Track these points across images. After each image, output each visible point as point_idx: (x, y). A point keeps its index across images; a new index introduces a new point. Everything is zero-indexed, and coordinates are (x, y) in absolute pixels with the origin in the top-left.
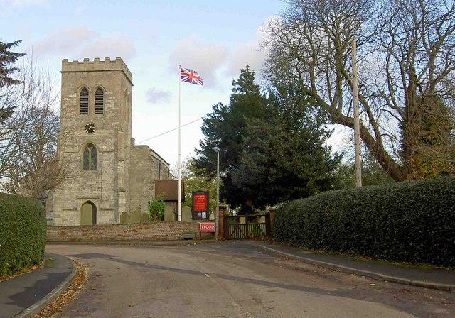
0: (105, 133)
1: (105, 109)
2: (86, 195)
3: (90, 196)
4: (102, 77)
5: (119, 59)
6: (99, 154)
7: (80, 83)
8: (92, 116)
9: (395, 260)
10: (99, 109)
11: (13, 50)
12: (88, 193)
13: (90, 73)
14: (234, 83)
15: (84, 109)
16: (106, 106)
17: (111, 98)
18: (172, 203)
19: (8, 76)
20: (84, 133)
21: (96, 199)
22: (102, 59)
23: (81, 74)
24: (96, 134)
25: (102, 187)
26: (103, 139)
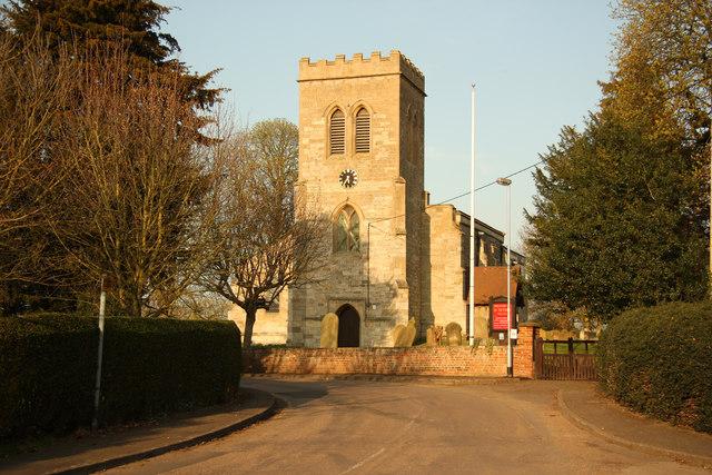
0: (374, 186)
1: (373, 146)
2: (341, 295)
3: (348, 296)
4: (338, 90)
7: (331, 100)
8: (348, 161)
9: (380, 180)
10: (362, 146)
11: (209, 86)
13: (347, 81)
14: (220, 101)
16: (374, 139)
17: (382, 124)
18: (483, 308)
19: (203, 131)
20: (338, 187)
21: (359, 300)
23: (319, 82)
24: (360, 187)
26: (370, 196)
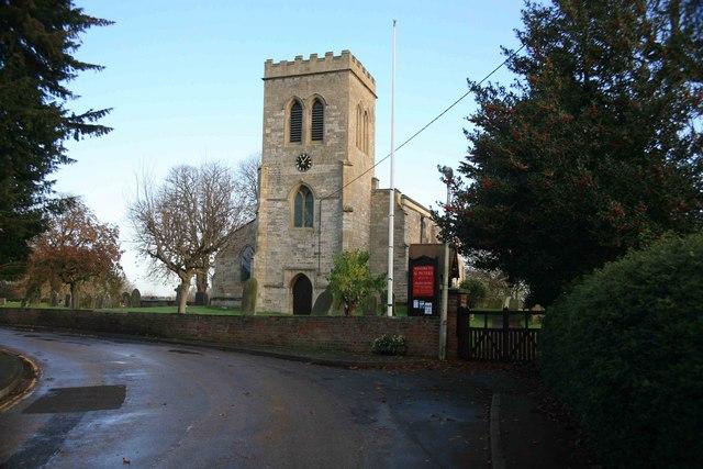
5: (346, 53)
6: (316, 202)
10: (318, 134)
12: (299, 262)
15: (296, 135)
22: (321, 55)
25: (319, 253)
